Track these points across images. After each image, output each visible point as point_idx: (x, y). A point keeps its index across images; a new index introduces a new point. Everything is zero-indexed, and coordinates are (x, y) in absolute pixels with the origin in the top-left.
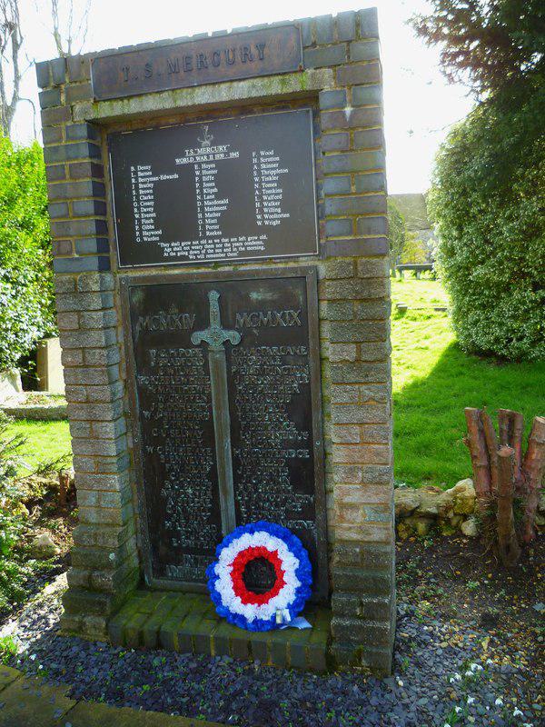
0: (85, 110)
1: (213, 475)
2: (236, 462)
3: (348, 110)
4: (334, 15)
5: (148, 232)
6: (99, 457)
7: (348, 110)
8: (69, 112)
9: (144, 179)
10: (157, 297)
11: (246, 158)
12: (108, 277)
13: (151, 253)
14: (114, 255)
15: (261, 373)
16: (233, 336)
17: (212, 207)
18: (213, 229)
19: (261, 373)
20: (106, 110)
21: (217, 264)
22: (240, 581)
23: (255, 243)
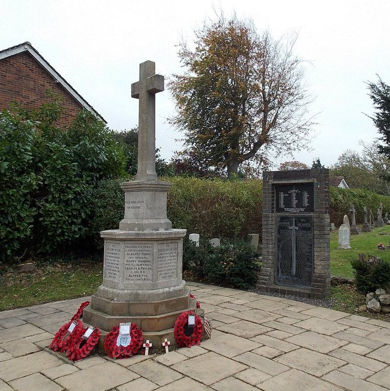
0: (271, 182)
1: (291, 259)
2: (296, 255)
3: (319, 186)
4: (119, 132)
5: (282, 206)
6: (212, 203)
7: (319, 186)
8: (268, 182)
9: (282, 195)
10: (283, 219)
11: (301, 193)
12: (273, 214)
13: (282, 210)
14: (275, 210)
15: (302, 236)
16: (297, 228)
17: (295, 202)
18: (295, 206)
19: (302, 236)
20: (275, 182)
21: (295, 213)
22: (303, 299)
23: (303, 210)
